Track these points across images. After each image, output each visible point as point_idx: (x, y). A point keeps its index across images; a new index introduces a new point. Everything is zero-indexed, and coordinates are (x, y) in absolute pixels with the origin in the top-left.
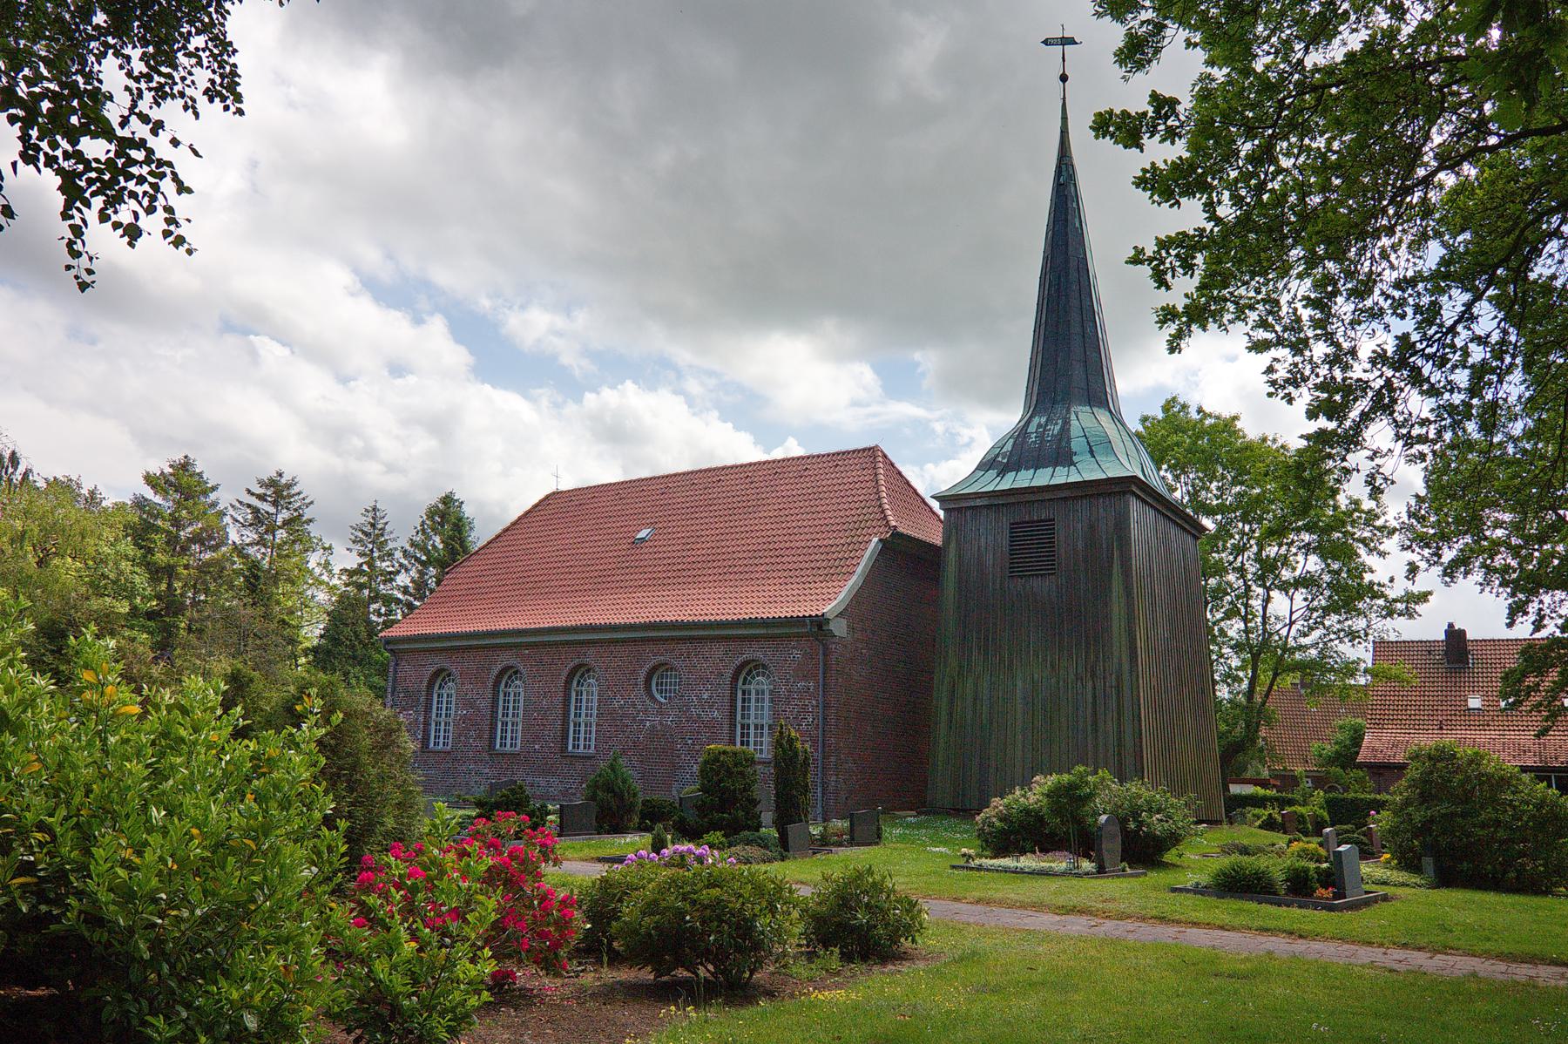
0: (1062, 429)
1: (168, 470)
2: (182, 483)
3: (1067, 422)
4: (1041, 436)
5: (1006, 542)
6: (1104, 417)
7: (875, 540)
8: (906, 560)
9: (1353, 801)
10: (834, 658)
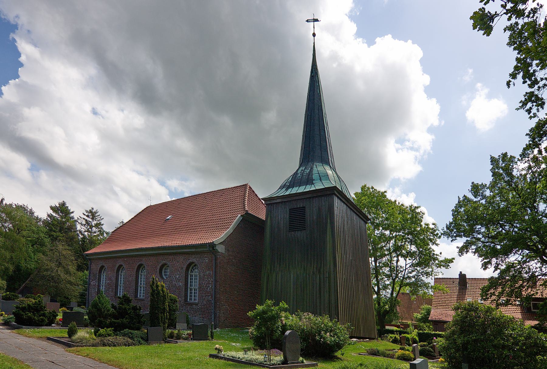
0: (310, 170)
1: (58, 205)
2: (62, 209)
3: (312, 168)
4: (302, 174)
5: (288, 217)
6: (327, 168)
7: (239, 215)
8: (249, 222)
9: (427, 334)
10: (219, 261)
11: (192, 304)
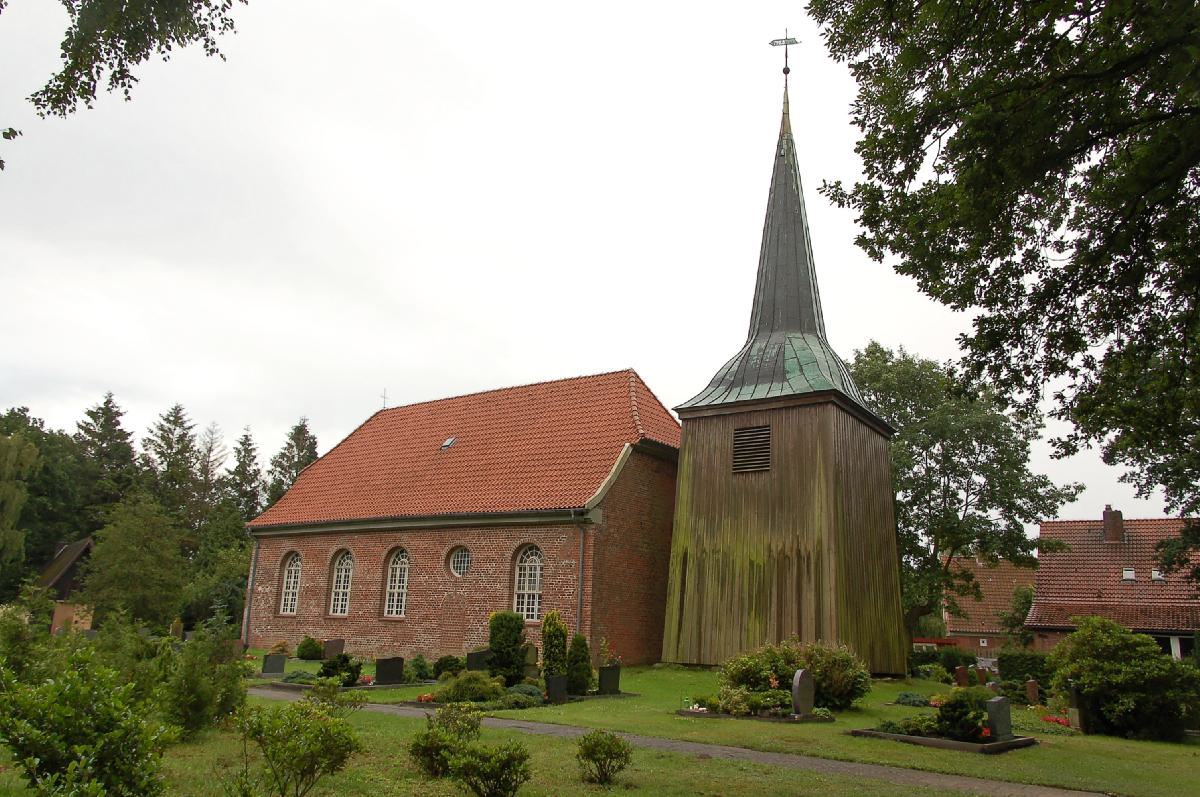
7: (627, 445)
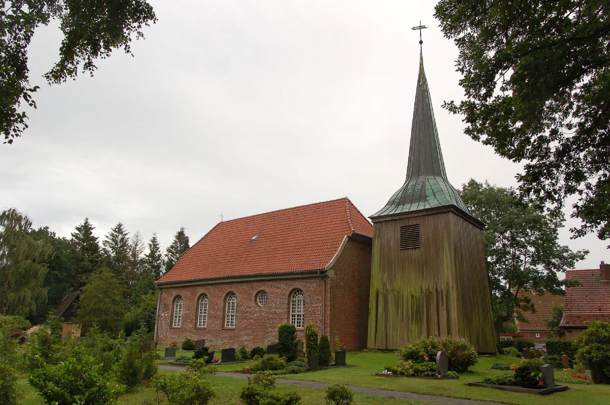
7: (346, 236)
11: (200, 329)
